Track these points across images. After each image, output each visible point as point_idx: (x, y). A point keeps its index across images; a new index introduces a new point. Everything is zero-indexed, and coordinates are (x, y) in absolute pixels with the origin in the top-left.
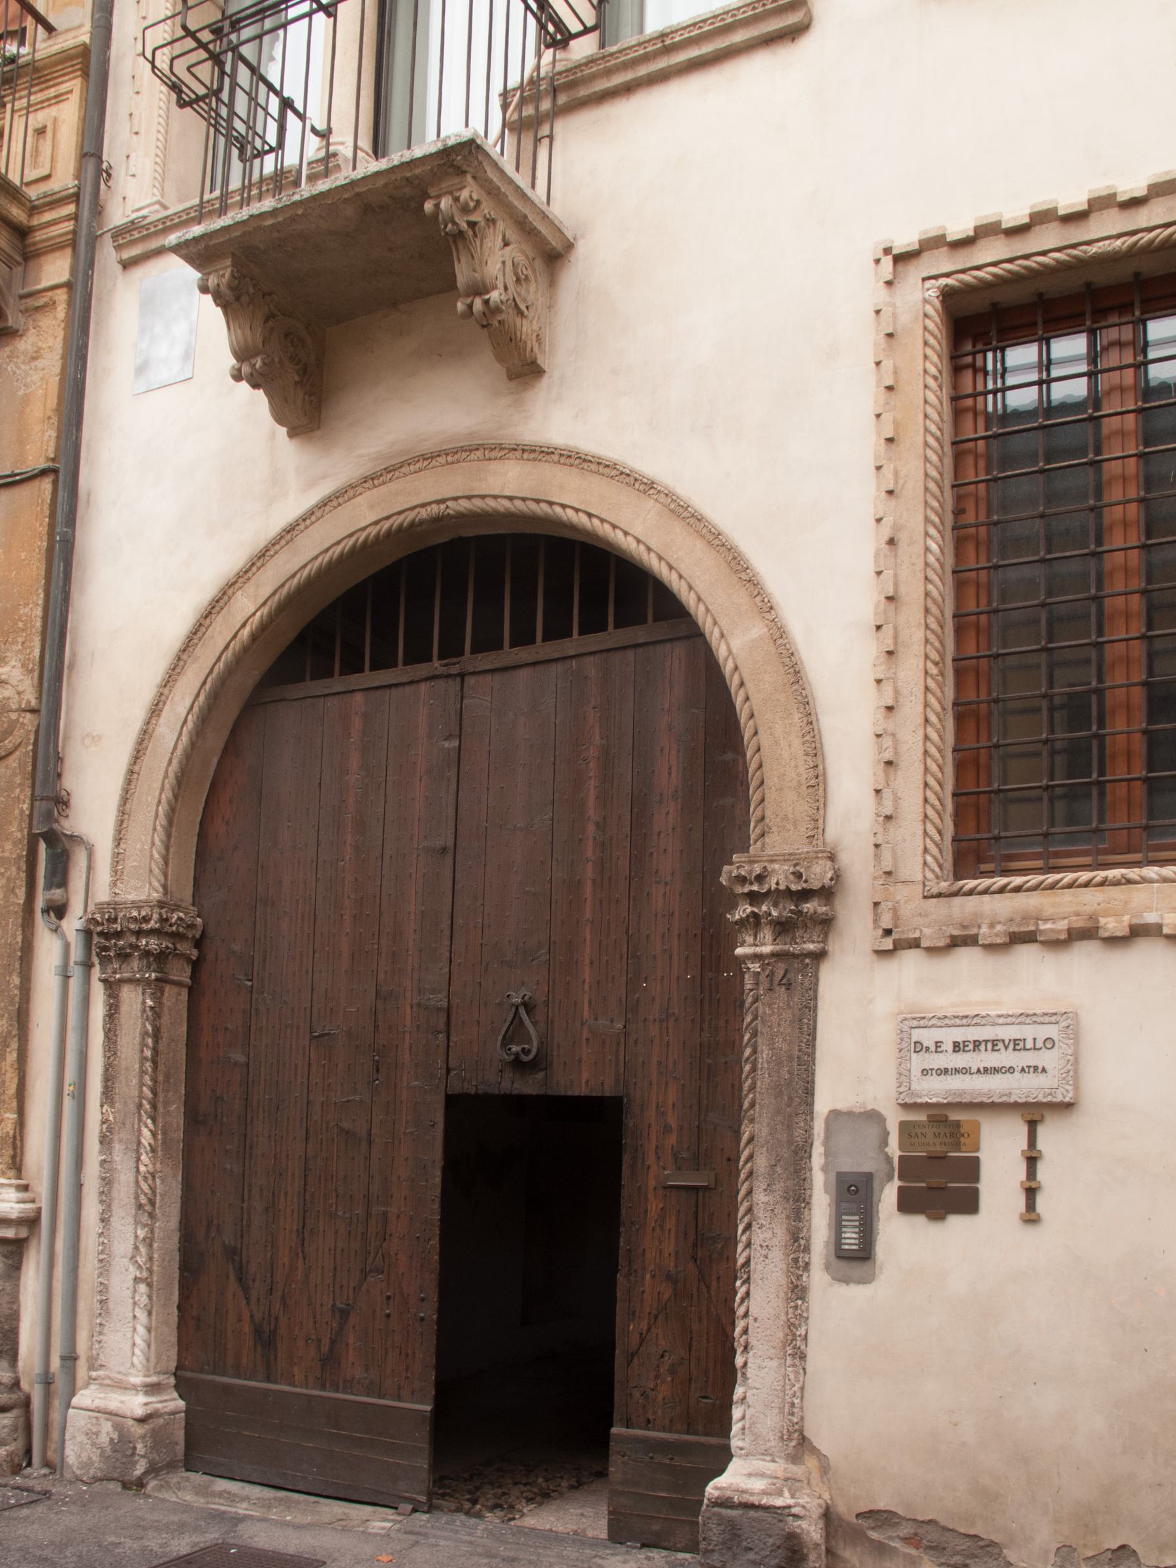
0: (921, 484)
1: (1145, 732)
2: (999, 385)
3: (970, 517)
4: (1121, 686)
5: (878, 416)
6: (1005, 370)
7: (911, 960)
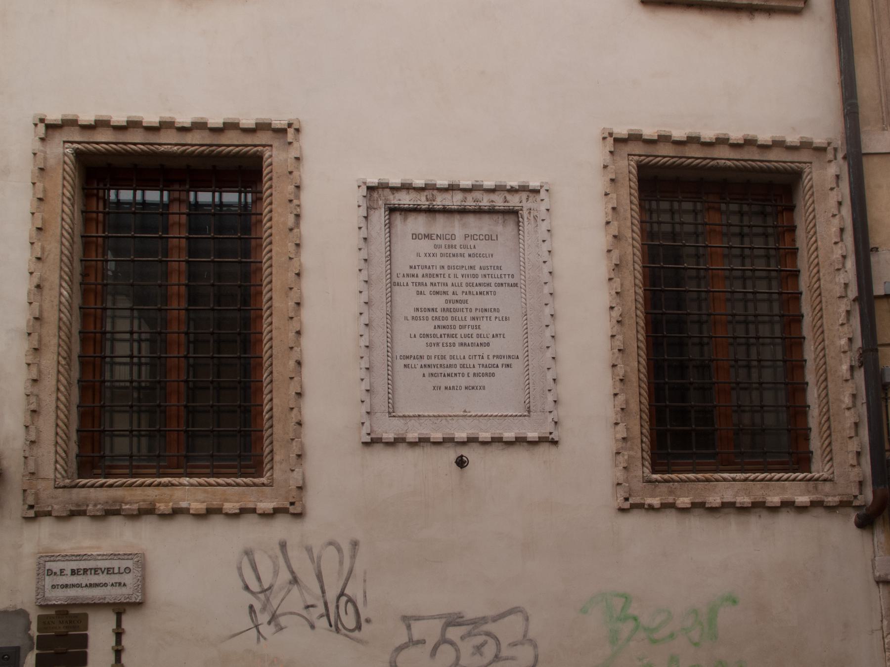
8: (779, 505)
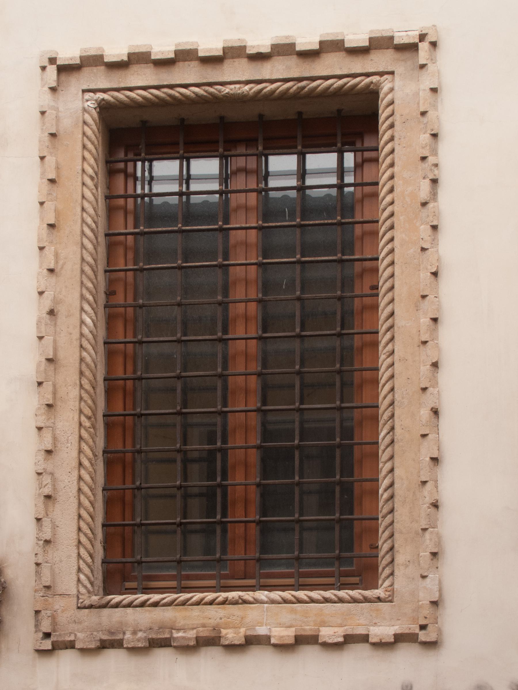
0: (78, 267)
1: (258, 485)
2: (147, 191)
3: (119, 299)
4: (241, 448)
5: (42, 204)
6: (152, 178)
7: (67, 659)
8: (292, 641)
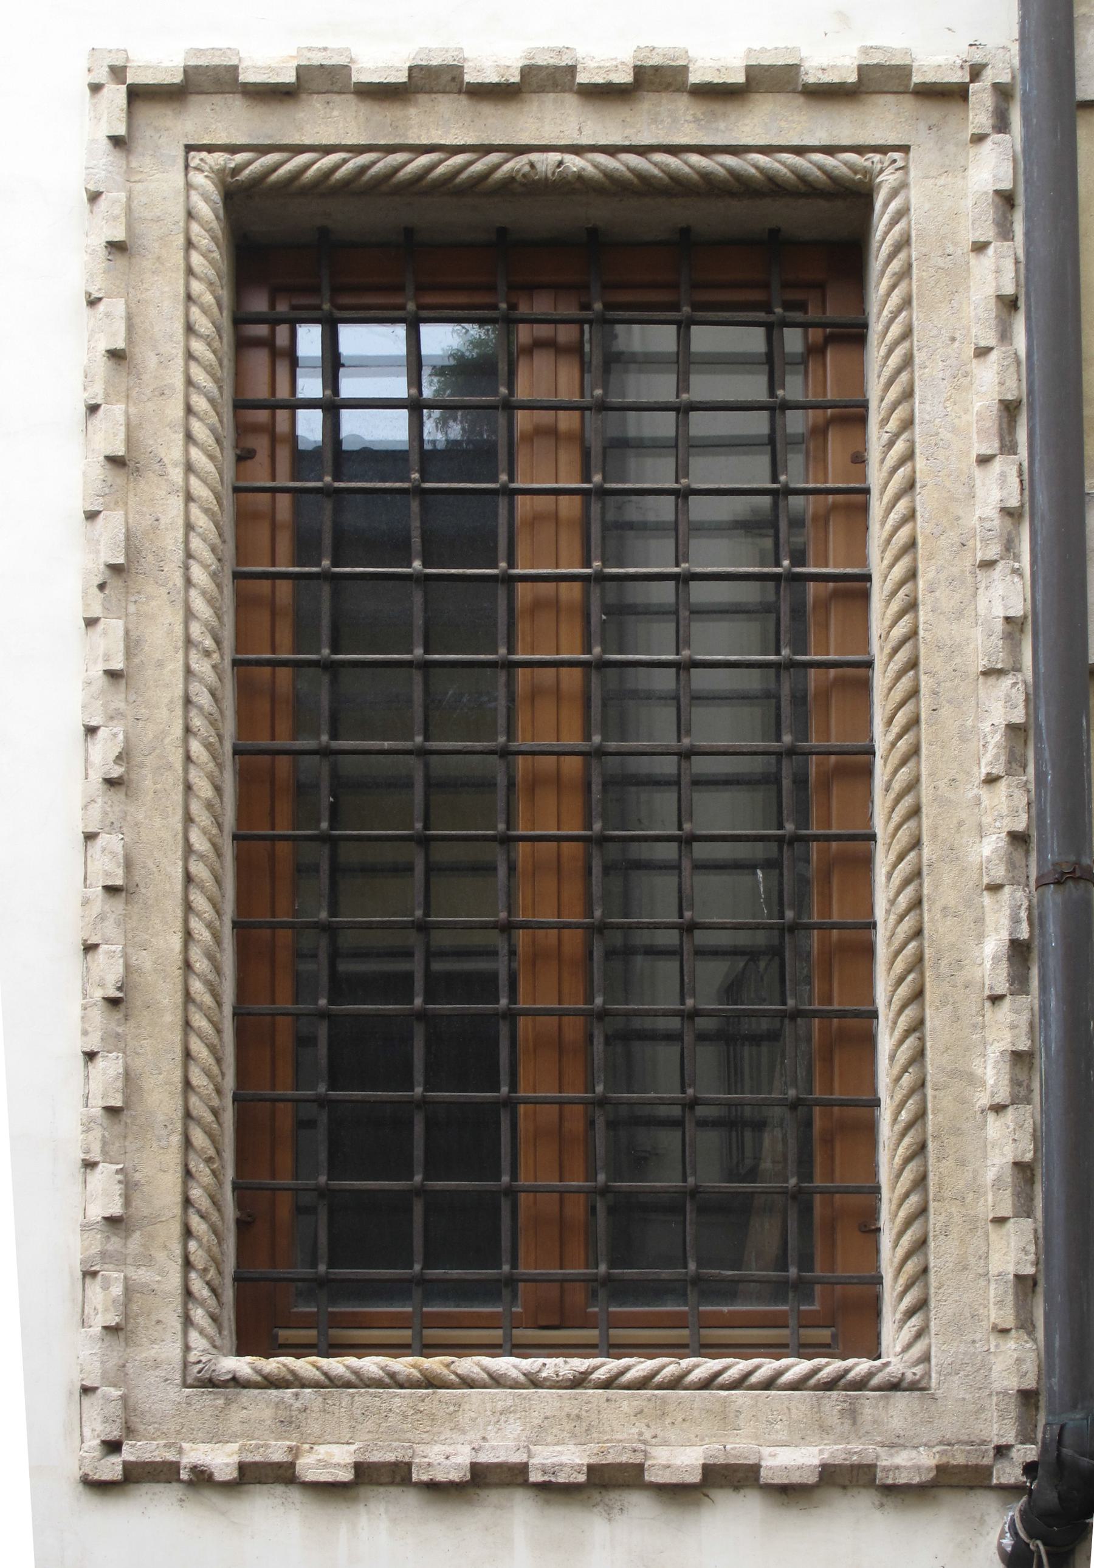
8: (696, 1477)
